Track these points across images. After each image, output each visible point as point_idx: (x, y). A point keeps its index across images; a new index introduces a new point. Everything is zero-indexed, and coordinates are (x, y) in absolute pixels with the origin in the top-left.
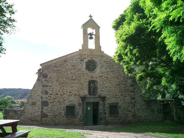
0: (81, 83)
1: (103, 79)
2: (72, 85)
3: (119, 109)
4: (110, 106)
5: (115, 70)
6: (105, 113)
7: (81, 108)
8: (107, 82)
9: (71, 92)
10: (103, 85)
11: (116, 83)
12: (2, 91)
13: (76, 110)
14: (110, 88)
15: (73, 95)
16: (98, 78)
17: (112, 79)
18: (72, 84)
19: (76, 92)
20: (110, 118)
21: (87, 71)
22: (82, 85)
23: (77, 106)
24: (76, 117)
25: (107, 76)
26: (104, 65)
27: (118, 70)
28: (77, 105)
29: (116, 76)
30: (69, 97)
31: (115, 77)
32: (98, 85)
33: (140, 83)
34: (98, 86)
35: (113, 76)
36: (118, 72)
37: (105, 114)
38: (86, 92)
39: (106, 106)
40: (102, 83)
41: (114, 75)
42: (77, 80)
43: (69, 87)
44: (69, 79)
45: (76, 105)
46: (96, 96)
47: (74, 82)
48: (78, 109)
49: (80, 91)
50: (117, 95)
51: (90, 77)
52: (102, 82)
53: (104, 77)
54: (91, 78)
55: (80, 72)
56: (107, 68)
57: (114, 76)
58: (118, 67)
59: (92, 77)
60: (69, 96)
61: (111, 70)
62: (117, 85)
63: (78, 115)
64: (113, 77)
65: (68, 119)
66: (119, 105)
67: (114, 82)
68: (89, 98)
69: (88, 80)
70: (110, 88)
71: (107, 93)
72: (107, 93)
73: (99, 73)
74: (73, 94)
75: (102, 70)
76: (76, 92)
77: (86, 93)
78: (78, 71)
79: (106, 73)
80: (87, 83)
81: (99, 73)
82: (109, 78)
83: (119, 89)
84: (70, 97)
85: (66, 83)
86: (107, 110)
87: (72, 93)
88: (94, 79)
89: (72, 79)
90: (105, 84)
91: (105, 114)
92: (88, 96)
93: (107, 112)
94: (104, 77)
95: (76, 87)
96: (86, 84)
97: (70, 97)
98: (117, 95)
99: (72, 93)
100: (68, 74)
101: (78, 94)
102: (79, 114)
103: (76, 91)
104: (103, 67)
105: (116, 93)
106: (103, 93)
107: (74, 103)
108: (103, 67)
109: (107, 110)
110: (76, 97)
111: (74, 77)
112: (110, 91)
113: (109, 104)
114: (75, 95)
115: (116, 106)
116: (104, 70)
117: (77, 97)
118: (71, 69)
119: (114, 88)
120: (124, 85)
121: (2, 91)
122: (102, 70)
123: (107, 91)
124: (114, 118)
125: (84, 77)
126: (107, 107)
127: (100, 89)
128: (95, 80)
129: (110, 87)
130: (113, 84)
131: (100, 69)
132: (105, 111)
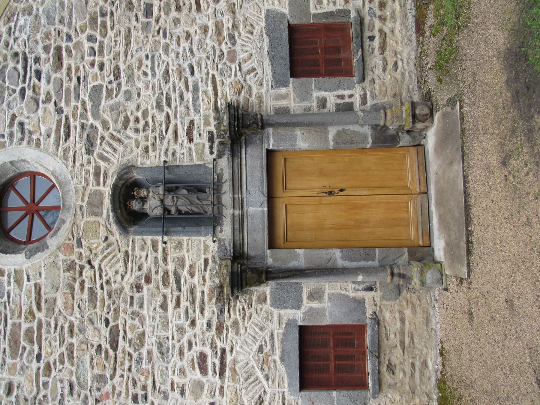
0: (139, 288)
1: (105, 125)
2: (149, 353)
3: (313, 11)
4: (293, 74)
5: (47, 36)
6: (339, 108)
7: (308, 285)
8: (128, 96)
9: (203, 357)
10: (146, 124)
11: (134, 33)
12: (274, 273)
13: (327, 321)
14: (167, 72)
15: (220, 344)
16: (102, 164)
17: (106, 59)
18: (144, 352)
19: (201, 322)
20: (378, 71)
21: (53, 242)
22: (148, 279)
23: (299, 317)
24: (377, 321)
25: (85, 96)
26: (14, 117)
27: (48, 17)
28: (288, 314)
29: (89, 31)
30: (233, 370)
31: (91, 39)
32: (148, 163)
33: (44, 26)
34: (154, 160)
35: (87, 50)
36: (61, 22)
37: (349, 107)
38: (198, 252)
39: (295, 105)
40: (137, 130)
41: (78, 45)
42: (116, 318)
43: (164, 374)
44: (108, 373)
45: (290, 323)
46: (227, 175)
47: (129, 335)
48: (315, 305)
49: (192, 292)
50: (219, 27)
51: (92, 219)
52: (130, 132)
53: (91, 120)
54: (98, 214)
55: (59, 296)
56: (29, 93)
57: (87, 45)
58: (30, 19)
59: (94, 205)
60: (228, 372)
61: (45, 68)
62: (146, 27)
63: (361, 303)
64: (93, 52)
65: (387, 378)
66: (286, 11)
67: (128, 45)
68: (239, 224)
69: (116, 235)
70: (167, 72)
71: (205, 92)
72: (205, 92)
73: (66, 151)
74: (213, 344)
75: (43, 129)
76: (201, 322)
77: (206, 248)
78: (51, 310)
79: (67, 103)
80: (138, 238)
81: (66, 159)
82: (99, 82)
83: (174, 14)
84: (235, 362)
85: (140, 393)
86: (322, 94)
87: (208, 350)
88: (107, 190)
89: (111, 352)
90: (145, 113)
91: (349, 107)
92: (226, 231)
93: (332, 99)
94: (91, 120)
95: (165, 325)
96: (144, 246)
97: (235, 362)
98: (219, 27)
99: (208, 350)
100: (71, 386)
101: (211, 307)
102: (351, 294)
103: (193, 323)
104: (21, 124)
105: (205, 29)
106: (207, 123)
107: (279, 332)
108: (21, 124)
109: (322, 94)
110: (236, 323)
111: (95, 341)
112: (188, 74)
113: (279, 82)
114: (220, 329)
115: (292, 29)
116: (44, 121)
117: (236, 316)
118: (39, 358)
119: (166, 49)
120: (72, 138)
121: (274, 273)
122: (43, 129)
123: (188, 96)
124: (376, 43)
125: (96, 264)
126: (304, 95)
127: (177, 148)
128: (111, 181)
129: (159, 73)
130: (142, 54)
131: (38, 145)
132: (331, 106)
